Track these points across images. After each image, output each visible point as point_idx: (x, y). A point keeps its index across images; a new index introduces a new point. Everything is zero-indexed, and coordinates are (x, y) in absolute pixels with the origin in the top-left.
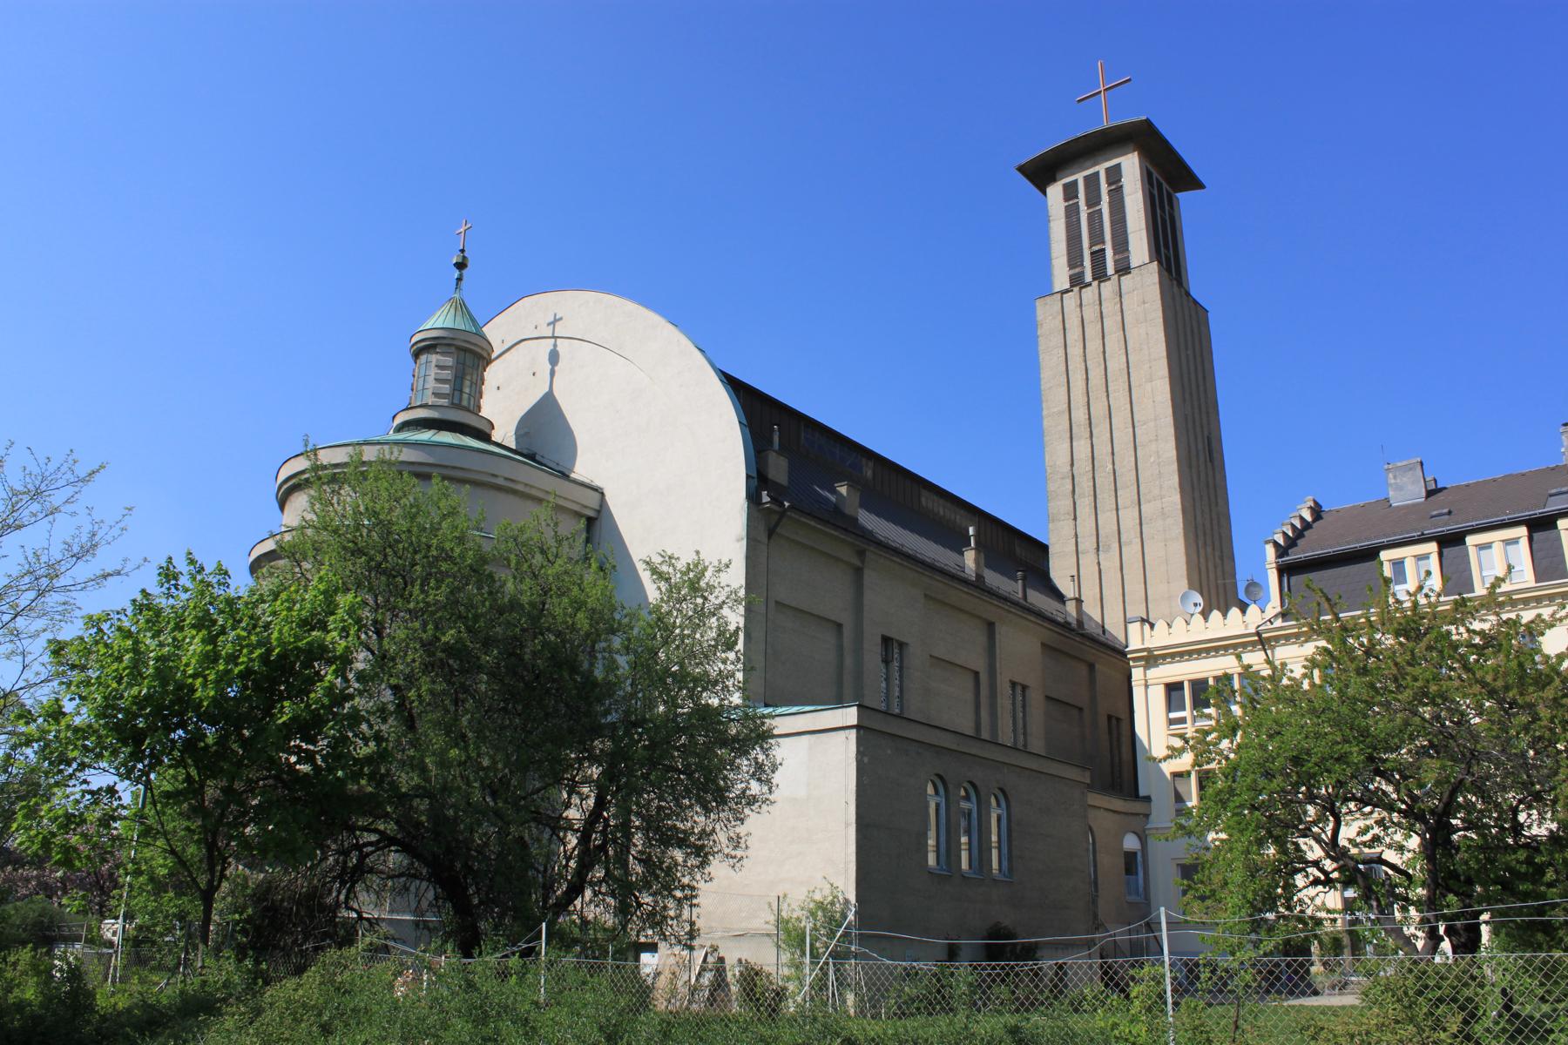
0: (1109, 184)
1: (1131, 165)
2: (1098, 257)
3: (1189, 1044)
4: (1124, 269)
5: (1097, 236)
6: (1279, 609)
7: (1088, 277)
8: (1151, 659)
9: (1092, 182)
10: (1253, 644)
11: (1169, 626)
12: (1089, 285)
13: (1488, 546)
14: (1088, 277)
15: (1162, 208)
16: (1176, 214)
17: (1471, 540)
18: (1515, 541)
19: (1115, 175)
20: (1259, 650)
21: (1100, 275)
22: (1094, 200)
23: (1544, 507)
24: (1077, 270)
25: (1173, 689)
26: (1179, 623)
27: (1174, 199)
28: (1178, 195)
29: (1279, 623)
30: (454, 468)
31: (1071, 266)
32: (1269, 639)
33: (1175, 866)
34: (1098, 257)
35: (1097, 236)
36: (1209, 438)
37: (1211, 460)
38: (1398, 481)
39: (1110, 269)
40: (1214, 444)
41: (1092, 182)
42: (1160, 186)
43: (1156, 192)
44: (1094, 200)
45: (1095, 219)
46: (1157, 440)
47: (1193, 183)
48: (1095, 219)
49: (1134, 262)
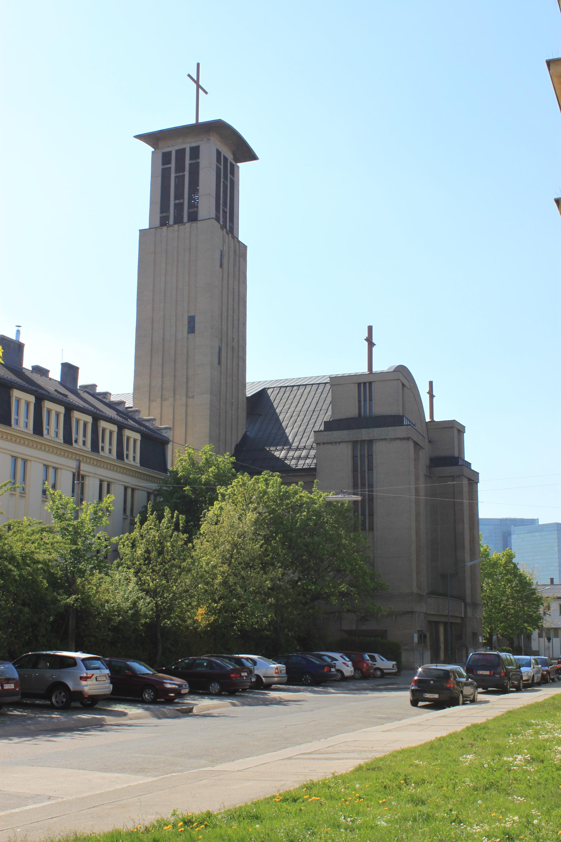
0: (191, 159)
4: (193, 217)
12: (171, 226)
16: (235, 180)
19: (195, 152)
21: (179, 220)
22: (180, 167)
27: (235, 168)
39: (185, 219)
42: (226, 159)
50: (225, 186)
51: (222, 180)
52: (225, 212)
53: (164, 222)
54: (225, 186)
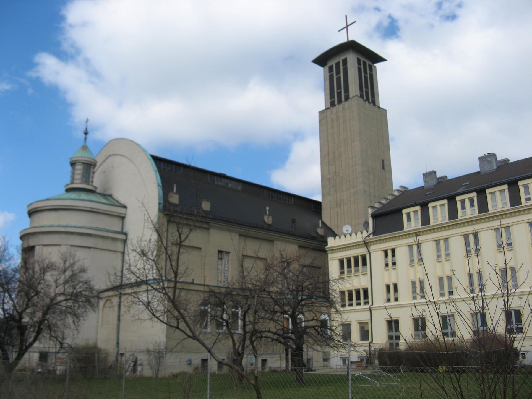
1: (352, 58)
2: (339, 94)
3: (528, 398)
5: (339, 87)
6: (372, 231)
7: (336, 102)
8: (335, 250)
10: (361, 244)
11: (356, 234)
13: (494, 193)
14: (336, 102)
15: (365, 72)
17: (520, 183)
18: (444, 205)
19: (345, 61)
20: (364, 247)
21: (340, 102)
22: (338, 72)
23: (456, 191)
24: (333, 100)
25: (341, 262)
26: (359, 233)
28: (376, 65)
30: (42, 227)
31: (331, 99)
32: (368, 243)
33: (357, 323)
34: (339, 94)
35: (339, 87)
37: (383, 168)
38: (427, 179)
39: (343, 99)
40: (385, 162)
41: (338, 64)
42: (365, 63)
43: (362, 67)
44: (338, 72)
45: (339, 79)
46: (355, 165)
47: (380, 59)
48: (339, 79)
49: (351, 96)
50: (366, 78)
51: (363, 74)
53: (333, 104)
54: (366, 78)
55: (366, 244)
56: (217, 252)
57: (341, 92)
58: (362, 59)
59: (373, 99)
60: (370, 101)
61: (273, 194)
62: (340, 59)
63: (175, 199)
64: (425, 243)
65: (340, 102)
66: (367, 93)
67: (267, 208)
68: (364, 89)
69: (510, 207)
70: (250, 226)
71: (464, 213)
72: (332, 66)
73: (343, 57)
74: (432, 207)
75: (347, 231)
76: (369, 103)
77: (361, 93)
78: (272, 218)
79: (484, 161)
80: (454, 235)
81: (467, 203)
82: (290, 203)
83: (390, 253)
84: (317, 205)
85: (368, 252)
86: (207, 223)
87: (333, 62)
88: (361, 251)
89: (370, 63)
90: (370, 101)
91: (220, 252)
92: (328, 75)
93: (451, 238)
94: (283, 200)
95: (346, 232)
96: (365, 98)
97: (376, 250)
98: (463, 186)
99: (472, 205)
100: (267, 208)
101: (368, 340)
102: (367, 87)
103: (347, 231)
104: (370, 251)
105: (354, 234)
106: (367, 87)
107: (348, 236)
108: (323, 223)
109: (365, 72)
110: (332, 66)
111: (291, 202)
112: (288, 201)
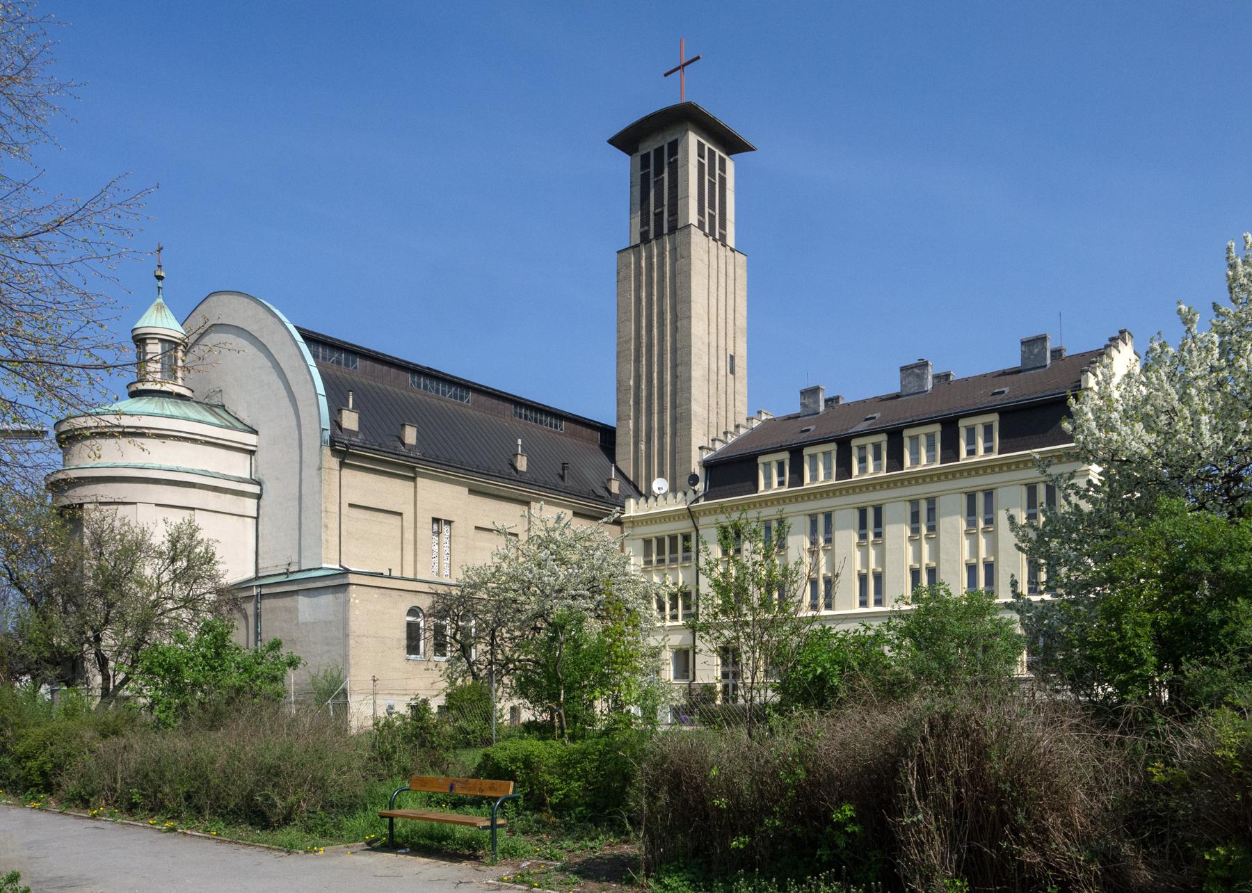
7: (652, 235)
9: (659, 152)
14: (652, 235)
15: (712, 174)
24: (646, 228)
29: (702, 502)
31: (676, 161)
34: (659, 216)
36: (732, 358)
39: (666, 231)
41: (659, 152)
42: (712, 153)
43: (706, 162)
44: (659, 171)
50: (712, 185)
51: (707, 177)
52: (712, 217)
53: (645, 239)
54: (712, 185)
55: (691, 514)
56: (431, 521)
57: (662, 212)
58: (707, 145)
59: (723, 232)
60: (717, 237)
61: (528, 413)
62: (663, 140)
63: (350, 420)
64: (839, 512)
65: (659, 234)
66: (712, 217)
67: (520, 442)
68: (707, 210)
69: (941, 464)
70: (488, 474)
71: (863, 470)
72: (648, 154)
73: (670, 139)
74: (809, 455)
75: (659, 489)
76: (715, 240)
77: (701, 219)
78: (528, 459)
79: (910, 374)
80: (1005, 484)
81: (923, 440)
82: (558, 430)
83: (923, 507)
84: (607, 437)
85: (694, 529)
86: (413, 469)
87: (649, 147)
88: (684, 526)
89: (723, 155)
90: (717, 237)
91: (436, 520)
92: (639, 173)
93: (941, 497)
94: (546, 425)
95: (657, 492)
96: (707, 231)
97: (708, 526)
98: (866, 420)
99: (877, 457)
100: (520, 442)
101: (688, 677)
102: (712, 206)
103: (659, 489)
104: (699, 528)
105: (670, 496)
106: (712, 206)
107: (660, 499)
108: (617, 469)
109: (712, 174)
110: (648, 154)
111: (561, 430)
112: (556, 427)
